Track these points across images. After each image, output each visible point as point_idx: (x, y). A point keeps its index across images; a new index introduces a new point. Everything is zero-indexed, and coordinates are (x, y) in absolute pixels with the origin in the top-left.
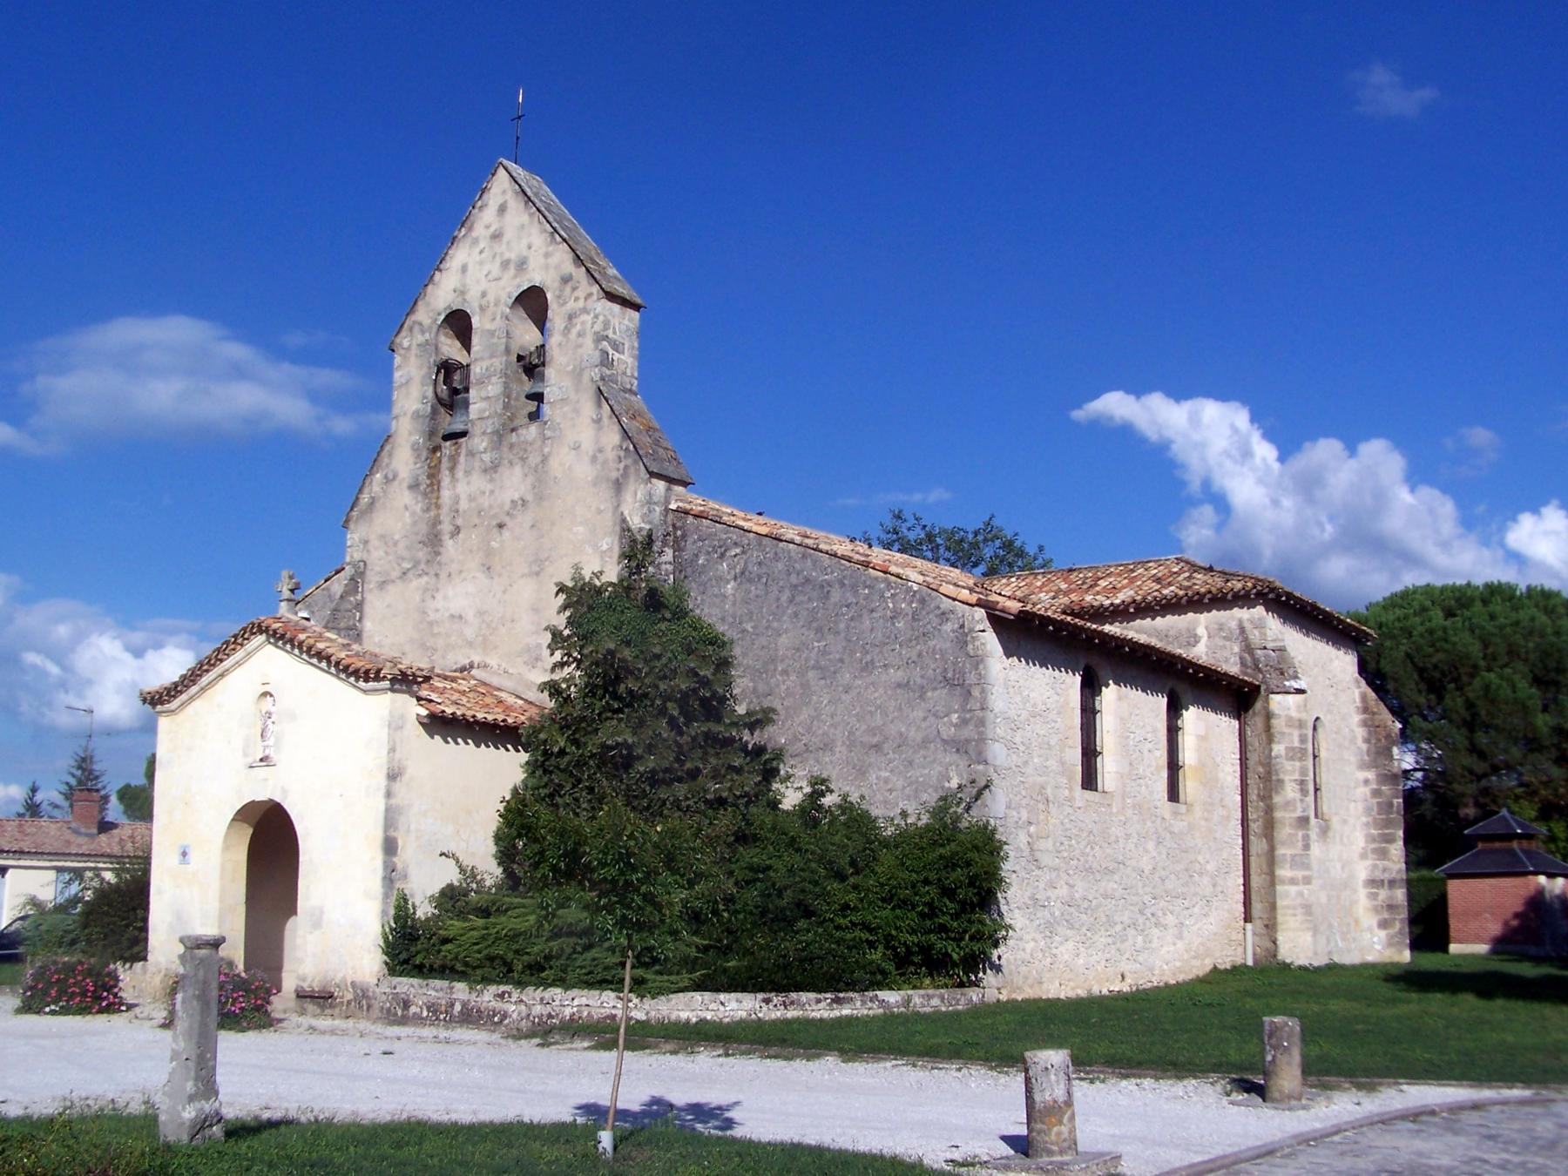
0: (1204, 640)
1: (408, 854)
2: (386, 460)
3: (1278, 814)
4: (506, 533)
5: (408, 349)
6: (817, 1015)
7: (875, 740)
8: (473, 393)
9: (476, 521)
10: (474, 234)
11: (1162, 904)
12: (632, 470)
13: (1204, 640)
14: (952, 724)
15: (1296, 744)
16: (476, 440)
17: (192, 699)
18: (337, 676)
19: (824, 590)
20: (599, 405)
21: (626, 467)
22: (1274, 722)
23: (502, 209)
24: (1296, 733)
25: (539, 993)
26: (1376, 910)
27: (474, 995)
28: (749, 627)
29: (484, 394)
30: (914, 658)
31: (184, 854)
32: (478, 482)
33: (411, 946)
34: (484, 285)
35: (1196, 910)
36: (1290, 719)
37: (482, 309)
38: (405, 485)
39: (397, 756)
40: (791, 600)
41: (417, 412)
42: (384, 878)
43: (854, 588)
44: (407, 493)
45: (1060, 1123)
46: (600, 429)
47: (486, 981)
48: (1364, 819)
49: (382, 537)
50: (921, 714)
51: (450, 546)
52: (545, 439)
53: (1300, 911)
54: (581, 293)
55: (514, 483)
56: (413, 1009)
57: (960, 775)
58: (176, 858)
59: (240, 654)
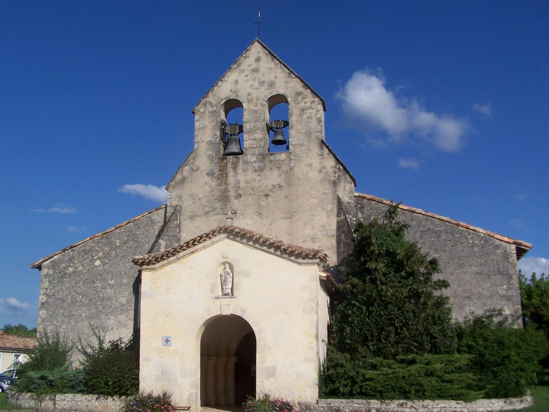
2: (192, 161)
4: (270, 199)
5: (204, 113)
7: (467, 295)
8: (245, 136)
9: (251, 192)
10: (242, 68)
12: (342, 177)
14: (504, 289)
18: (281, 256)
19: (438, 234)
20: (322, 148)
21: (339, 176)
23: (258, 60)
25: (421, 403)
27: (384, 405)
29: (252, 137)
30: (484, 262)
32: (251, 175)
34: (249, 90)
38: (204, 173)
40: (421, 237)
41: (211, 141)
43: (452, 234)
44: (206, 177)
47: (392, 398)
50: (489, 285)
51: (235, 203)
52: (291, 160)
55: (273, 177)
57: (509, 309)
58: (160, 343)
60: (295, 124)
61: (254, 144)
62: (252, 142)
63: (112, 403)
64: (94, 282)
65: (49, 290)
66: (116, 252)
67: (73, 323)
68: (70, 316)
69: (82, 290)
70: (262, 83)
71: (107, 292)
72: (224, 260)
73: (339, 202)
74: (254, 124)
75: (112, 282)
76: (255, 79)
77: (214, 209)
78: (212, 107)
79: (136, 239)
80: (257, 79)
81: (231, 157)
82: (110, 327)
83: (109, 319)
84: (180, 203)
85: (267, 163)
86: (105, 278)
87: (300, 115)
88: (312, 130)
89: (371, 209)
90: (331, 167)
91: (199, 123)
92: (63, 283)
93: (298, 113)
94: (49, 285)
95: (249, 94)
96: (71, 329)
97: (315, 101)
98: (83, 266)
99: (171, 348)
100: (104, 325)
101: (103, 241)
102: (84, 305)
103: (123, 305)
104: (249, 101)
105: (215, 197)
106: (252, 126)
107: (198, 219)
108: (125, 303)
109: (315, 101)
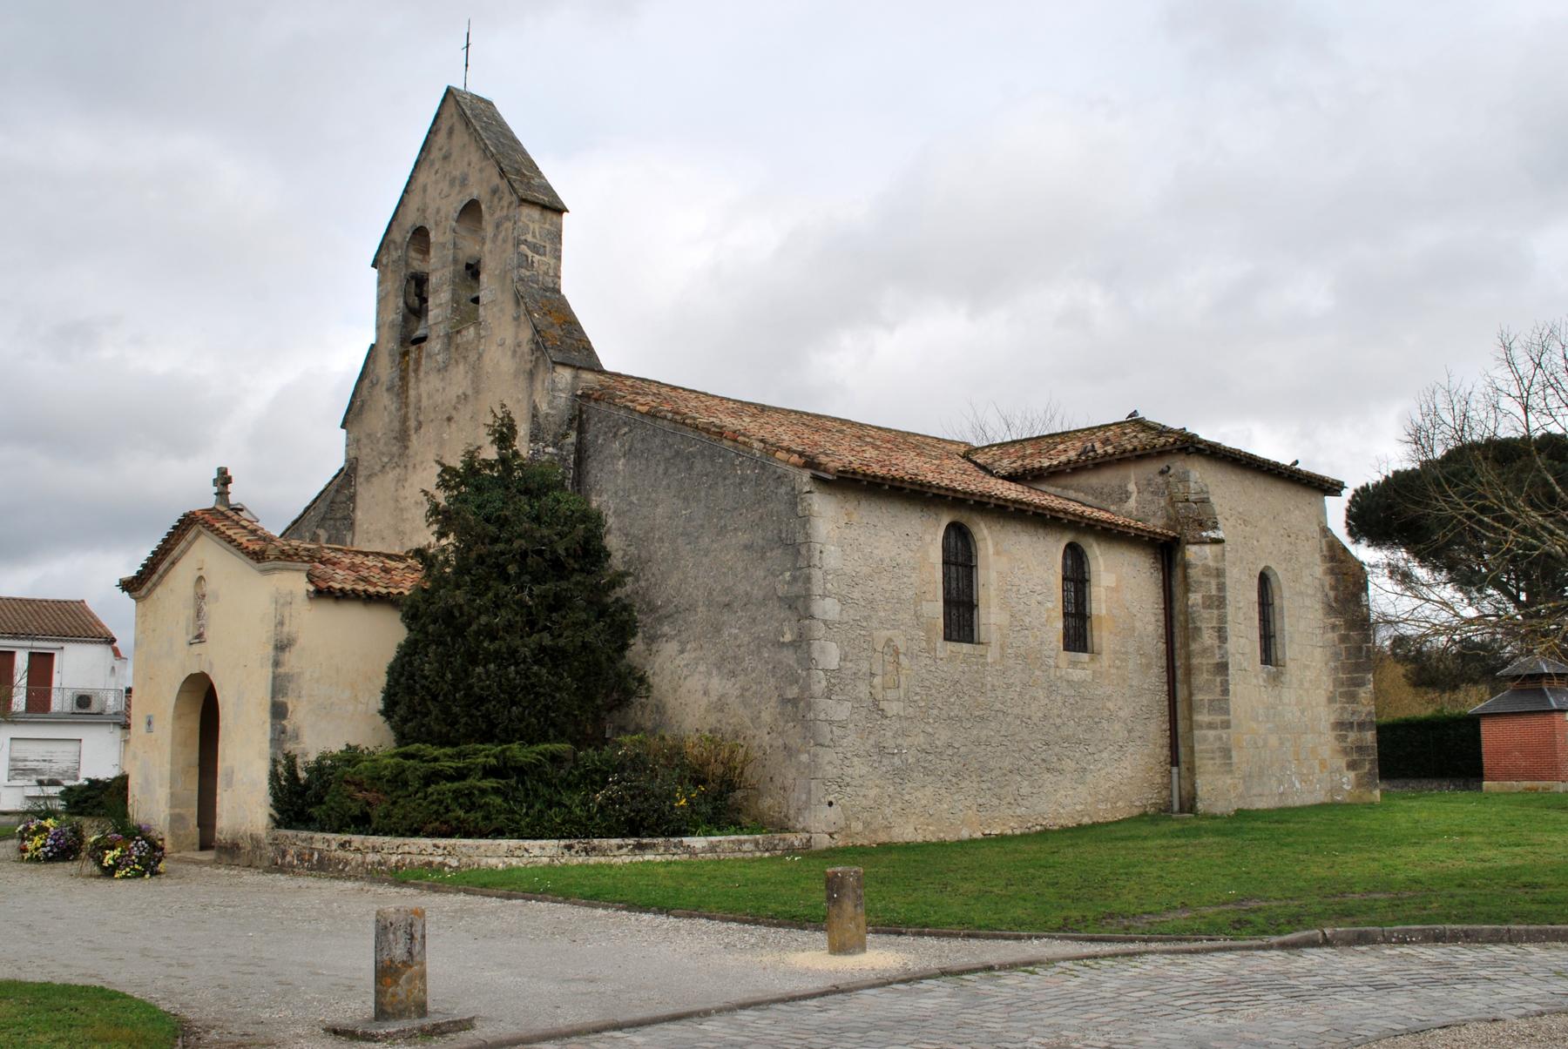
0: (1134, 496)
1: (300, 715)
3: (1195, 661)
4: (453, 426)
6: (618, 861)
11: (1057, 749)
13: (1134, 496)
15: (1214, 592)
16: (433, 343)
17: (155, 585)
22: (1191, 572)
23: (451, 132)
24: (1214, 583)
26: (1345, 752)
28: (634, 499)
31: (149, 723)
33: (303, 798)
35: (1105, 755)
36: (1206, 568)
37: (437, 224)
39: (286, 629)
42: (272, 740)
43: (712, 458)
45: (396, 983)
46: (518, 326)
48: (1332, 664)
49: (369, 436)
51: (415, 441)
53: (1218, 754)
54: (505, 203)
55: (459, 379)
56: (288, 858)
59: (183, 544)
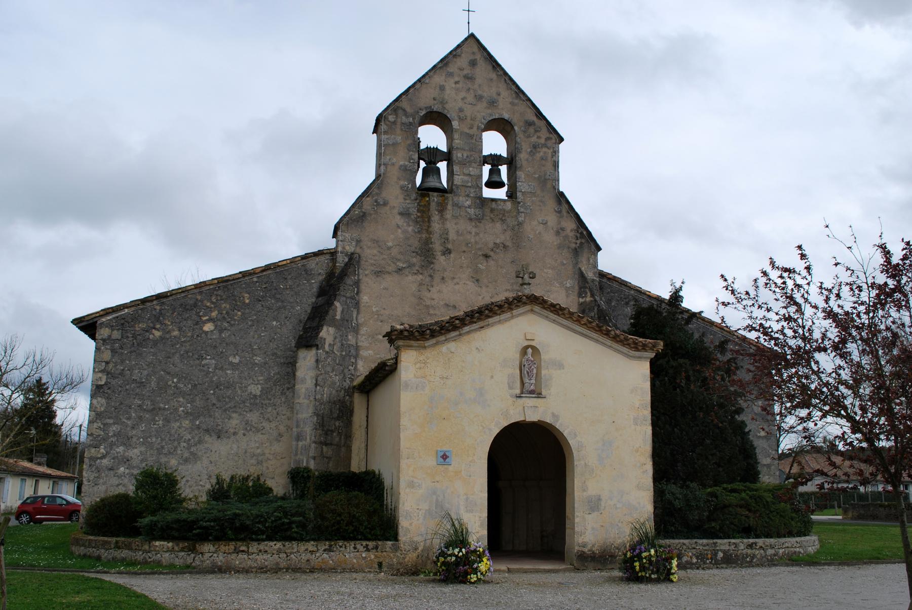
4: (491, 263)
5: (394, 123)
21: (581, 243)
29: (466, 171)
32: (464, 225)
38: (396, 211)
44: (399, 217)
52: (519, 212)
60: (524, 163)
61: (468, 182)
62: (466, 178)
63: (352, 555)
64: (201, 358)
65: (111, 366)
66: (243, 314)
67: (161, 422)
68: (155, 411)
69: (177, 369)
70: (479, 98)
71: (226, 374)
72: (527, 343)
73: (582, 276)
74: (469, 153)
75: (236, 360)
76: (469, 89)
77: (411, 266)
78: (407, 117)
79: (278, 296)
80: (471, 91)
81: (435, 194)
82: (232, 431)
83: (230, 418)
84: (358, 250)
85: (487, 211)
86: (222, 352)
87: (532, 154)
88: (547, 177)
89: (611, 291)
90: (571, 231)
91: (386, 136)
92: (141, 354)
93: (529, 150)
94: (113, 356)
95: (461, 110)
96: (157, 431)
97: (551, 138)
98: (180, 329)
99: (451, 468)
100: (220, 427)
101: (219, 292)
102: (183, 394)
103: (255, 396)
104: (461, 119)
105: (413, 249)
106: (465, 155)
107: (386, 276)
108: (259, 393)
109: (551, 138)
